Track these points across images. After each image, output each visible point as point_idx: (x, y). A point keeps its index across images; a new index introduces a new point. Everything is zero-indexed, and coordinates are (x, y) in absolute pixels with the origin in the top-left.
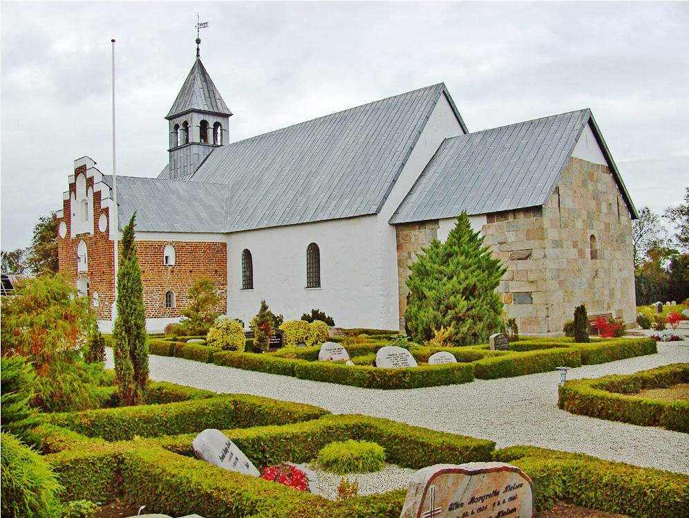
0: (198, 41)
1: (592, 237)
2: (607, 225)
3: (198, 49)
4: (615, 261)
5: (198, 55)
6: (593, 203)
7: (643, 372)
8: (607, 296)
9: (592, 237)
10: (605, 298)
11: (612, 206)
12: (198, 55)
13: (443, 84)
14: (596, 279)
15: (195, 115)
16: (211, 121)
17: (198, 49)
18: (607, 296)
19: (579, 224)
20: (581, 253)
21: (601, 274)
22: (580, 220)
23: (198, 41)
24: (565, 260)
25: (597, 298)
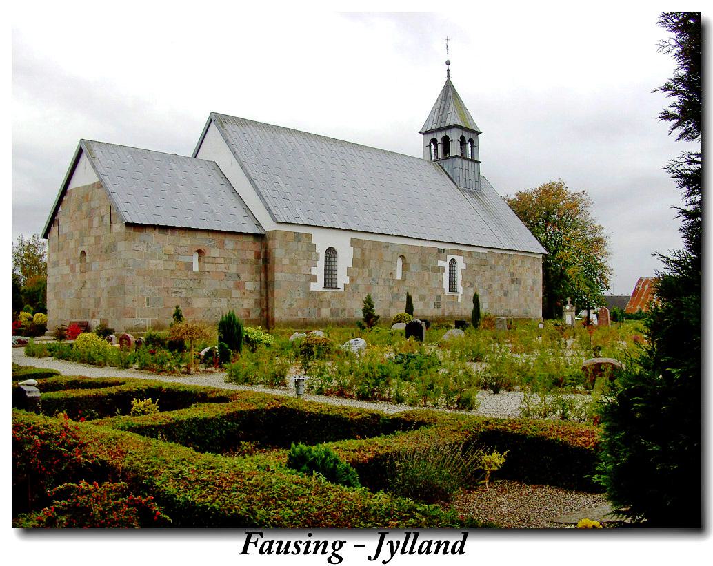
0: (448, 63)
1: (83, 252)
2: (98, 238)
3: (448, 70)
4: (104, 271)
5: (449, 76)
6: (85, 222)
7: (206, 372)
8: (92, 305)
9: (83, 252)
10: (90, 307)
11: (105, 218)
12: (449, 76)
13: (697, 16)
14: (83, 290)
15: (454, 131)
16: (467, 136)
17: (448, 70)
18: (92, 305)
19: (72, 244)
20: (73, 269)
21: (88, 285)
22: (73, 240)
23: (448, 63)
24: (60, 277)
25: (83, 307)
